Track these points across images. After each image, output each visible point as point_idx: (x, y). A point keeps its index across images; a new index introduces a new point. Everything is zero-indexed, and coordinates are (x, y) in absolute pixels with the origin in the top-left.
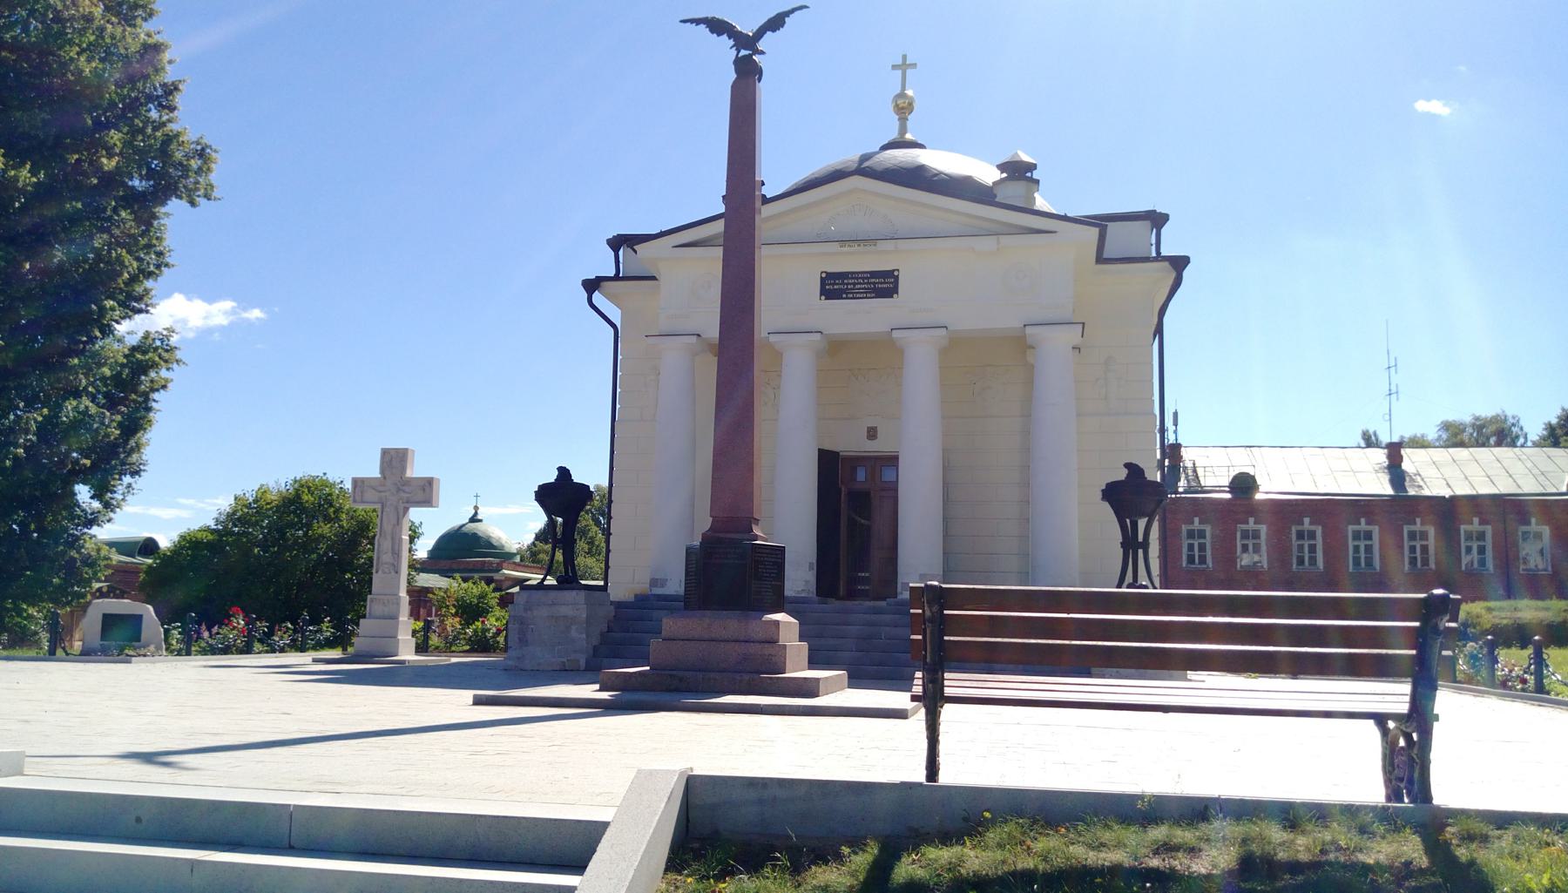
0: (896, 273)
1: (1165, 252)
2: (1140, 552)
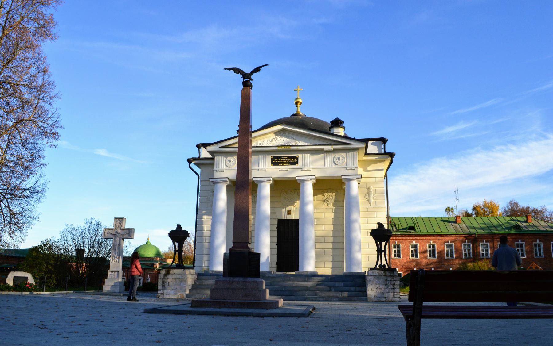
0: (297, 157)
1: (387, 152)
2: (383, 253)
